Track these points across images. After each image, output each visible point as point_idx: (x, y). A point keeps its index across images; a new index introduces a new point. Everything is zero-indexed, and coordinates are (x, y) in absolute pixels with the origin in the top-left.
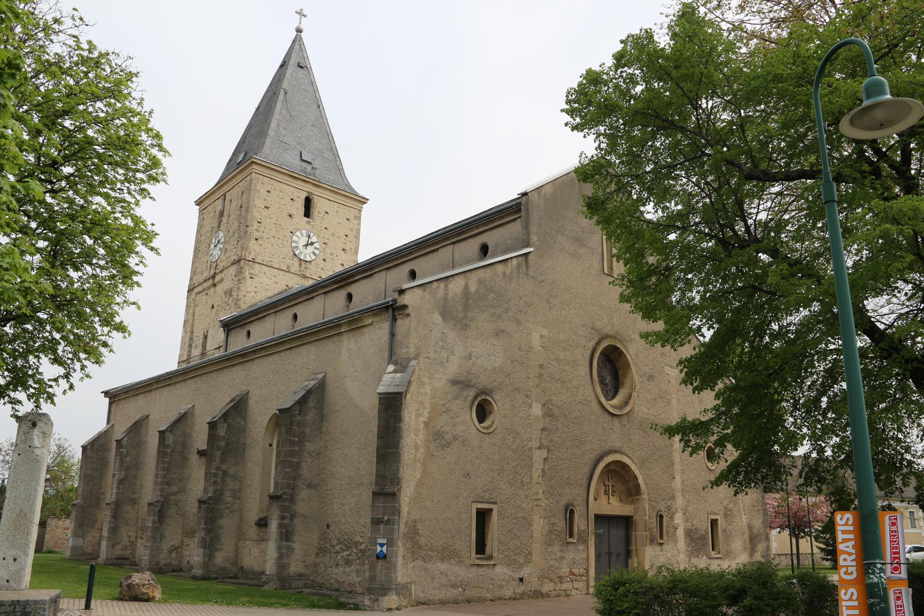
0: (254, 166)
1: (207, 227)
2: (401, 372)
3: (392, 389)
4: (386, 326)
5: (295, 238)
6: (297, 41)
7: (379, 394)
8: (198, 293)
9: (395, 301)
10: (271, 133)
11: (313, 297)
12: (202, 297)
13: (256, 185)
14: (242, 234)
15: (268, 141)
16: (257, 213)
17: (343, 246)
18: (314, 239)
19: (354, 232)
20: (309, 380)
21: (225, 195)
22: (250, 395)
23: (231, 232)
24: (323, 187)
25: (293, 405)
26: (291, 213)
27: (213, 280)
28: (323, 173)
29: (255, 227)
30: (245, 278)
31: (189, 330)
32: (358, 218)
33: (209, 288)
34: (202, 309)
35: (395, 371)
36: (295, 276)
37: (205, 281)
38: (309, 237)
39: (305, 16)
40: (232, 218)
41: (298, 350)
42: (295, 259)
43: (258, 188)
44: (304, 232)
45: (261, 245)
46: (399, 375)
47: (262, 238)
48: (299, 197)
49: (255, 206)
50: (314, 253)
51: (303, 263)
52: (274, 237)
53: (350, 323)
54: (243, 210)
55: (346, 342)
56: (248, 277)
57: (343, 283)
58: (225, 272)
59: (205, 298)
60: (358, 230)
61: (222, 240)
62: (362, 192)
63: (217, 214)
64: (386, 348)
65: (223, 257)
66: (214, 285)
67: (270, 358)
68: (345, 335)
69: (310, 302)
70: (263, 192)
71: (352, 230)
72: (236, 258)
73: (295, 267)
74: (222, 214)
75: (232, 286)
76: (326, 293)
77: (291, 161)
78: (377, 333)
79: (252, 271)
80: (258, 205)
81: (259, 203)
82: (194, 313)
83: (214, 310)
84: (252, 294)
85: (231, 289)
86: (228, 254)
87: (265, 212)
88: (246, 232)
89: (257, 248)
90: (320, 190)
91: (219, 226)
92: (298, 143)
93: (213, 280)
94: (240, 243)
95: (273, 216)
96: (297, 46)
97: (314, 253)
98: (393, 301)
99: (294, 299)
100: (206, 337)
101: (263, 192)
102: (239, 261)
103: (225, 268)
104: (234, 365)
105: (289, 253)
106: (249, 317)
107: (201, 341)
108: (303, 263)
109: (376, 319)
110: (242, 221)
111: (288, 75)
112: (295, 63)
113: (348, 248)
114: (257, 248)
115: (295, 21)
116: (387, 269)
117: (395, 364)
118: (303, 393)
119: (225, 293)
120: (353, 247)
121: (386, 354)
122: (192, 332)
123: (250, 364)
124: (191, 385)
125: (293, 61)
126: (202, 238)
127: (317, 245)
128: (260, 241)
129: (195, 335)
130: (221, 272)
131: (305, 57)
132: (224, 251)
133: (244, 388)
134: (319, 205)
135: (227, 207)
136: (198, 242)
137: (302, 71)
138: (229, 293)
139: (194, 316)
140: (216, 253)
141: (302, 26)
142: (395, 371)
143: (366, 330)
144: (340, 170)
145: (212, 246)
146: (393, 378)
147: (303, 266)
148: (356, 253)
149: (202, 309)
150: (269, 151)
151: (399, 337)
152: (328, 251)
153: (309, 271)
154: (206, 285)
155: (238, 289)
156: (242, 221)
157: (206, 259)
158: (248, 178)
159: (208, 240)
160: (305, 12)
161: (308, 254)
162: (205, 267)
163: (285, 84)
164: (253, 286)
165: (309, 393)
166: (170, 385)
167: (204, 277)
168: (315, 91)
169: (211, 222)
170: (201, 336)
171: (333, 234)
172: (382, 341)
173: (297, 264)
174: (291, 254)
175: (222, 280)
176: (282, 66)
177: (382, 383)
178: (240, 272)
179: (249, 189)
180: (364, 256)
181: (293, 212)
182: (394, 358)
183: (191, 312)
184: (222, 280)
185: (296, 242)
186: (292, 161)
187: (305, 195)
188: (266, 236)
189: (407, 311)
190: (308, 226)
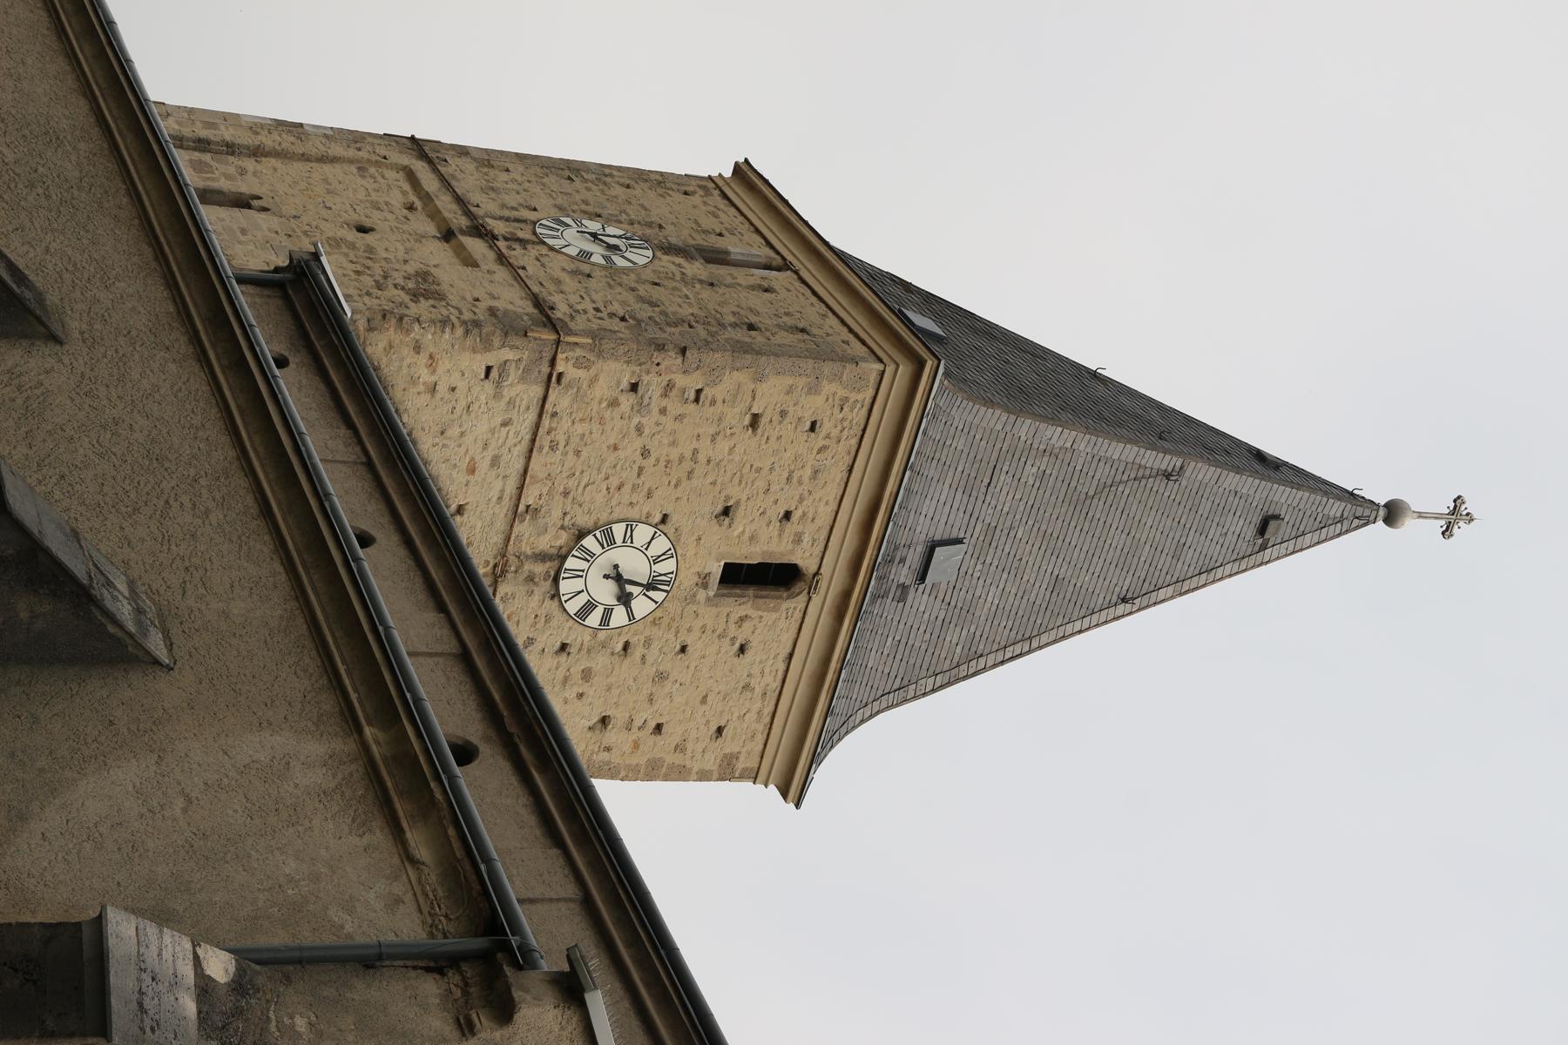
0: (905, 370)
1: (660, 208)
2: (202, 1017)
3: (121, 982)
4: (407, 927)
5: (643, 533)
6: (1352, 510)
7: (99, 922)
8: (411, 177)
9: (525, 959)
10: (1025, 428)
11: (441, 608)
12: (397, 192)
13: (837, 377)
14: (653, 332)
15: (994, 419)
16: (732, 384)
17: (619, 716)
18: (641, 606)
19: (672, 758)
20: (134, 595)
21: (785, 266)
22: (49, 349)
23: (656, 293)
24: (845, 628)
25: (18, 525)
26: (739, 514)
27: (465, 229)
28: (896, 623)
29: (680, 380)
30: (487, 346)
31: (268, 141)
32: (727, 771)
33: (434, 214)
34: (351, 192)
35: (204, 987)
36: (498, 539)
37: (459, 200)
38: (651, 586)
39: (1447, 532)
40: (706, 294)
41: (263, 546)
42: (563, 538)
43: (828, 388)
44: (668, 566)
45: (614, 403)
46: (190, 1007)
47: (641, 407)
48: (798, 539)
49: (759, 378)
50: (589, 607)
51: (550, 567)
52: (645, 453)
53: (404, 760)
54: (741, 335)
55: (316, 748)
56: (492, 358)
57: (512, 728)
58: (501, 274)
59: (396, 199)
60: (679, 773)
61: (619, 262)
62: (845, 766)
63: (714, 241)
64: (307, 937)
65: (556, 265)
66: (448, 235)
67: (215, 432)
68: (351, 746)
69: (422, 596)
70: (812, 406)
71: (680, 748)
72: (561, 311)
73: (536, 537)
74: (716, 257)
75: (453, 299)
76: (465, 657)
77: (928, 507)
78: (369, 891)
79: (513, 374)
80: (763, 388)
81: (771, 392)
82: (334, 160)
83: (352, 236)
84: (425, 376)
85: (440, 296)
86: (570, 284)
87: (736, 416)
88: (661, 347)
89: (602, 390)
90: (826, 620)
91: (669, 249)
92: (990, 530)
93: (465, 229)
94: (616, 325)
95: (724, 445)
96: (1336, 508)
97: (589, 607)
98: (526, 950)
99: (427, 533)
100: (242, 202)
101: (812, 406)
102: (551, 324)
103: (516, 272)
104: (171, 284)
105: (594, 511)
106: (340, 364)
107: (223, 184)
108: (550, 567)
109: (432, 876)
110: (701, 331)
111: (1232, 480)
112: (1273, 505)
113: (612, 736)
114: (602, 390)
115: (1430, 497)
116: (587, 903)
117: (239, 985)
118: (78, 569)
119: (424, 275)
120: (615, 758)
121: (276, 938)
122: (257, 152)
123: (183, 346)
124: (70, 113)
125: (1282, 496)
126: (618, 190)
127: (619, 617)
128: (627, 401)
129: (249, 164)
130: (501, 259)
131: (1298, 541)
132: (580, 266)
133: (74, 325)
134: (773, 623)
135: (741, 276)
136: (603, 174)
137: (1250, 532)
138: (425, 287)
139: (323, 159)
140: (572, 240)
141: (1409, 525)
142: (204, 987)
143: (379, 836)
144: (902, 691)
145: (594, 226)
146: (175, 983)
147: (540, 569)
148: (653, 771)
149: (351, 192)
150: (964, 423)
151: (365, 991)
152: (600, 661)
153: (521, 590)
154: (445, 203)
155: (445, 322)
156: (701, 331)
157: (544, 202)
158: (860, 350)
159: (611, 209)
160: (1461, 530)
161: (588, 583)
162: (511, 200)
163: (1200, 472)
164: (455, 379)
165: (80, 597)
166: (61, 32)
167: (475, 197)
168: (1181, 585)
169: (681, 220)
170: (244, 187)
171: (661, 677)
172: (336, 914)
173: (545, 543)
174: (584, 520)
175: (470, 262)
176: (1260, 456)
177: (151, 930)
178: (510, 328)
179: (822, 353)
180: (624, 803)
181: (742, 523)
182: (262, 976)
183: (337, 150)
184: (470, 262)
185: (628, 539)
186: (929, 510)
187: (807, 563)
188: (648, 422)
189: (483, 1021)
190: (688, 579)
